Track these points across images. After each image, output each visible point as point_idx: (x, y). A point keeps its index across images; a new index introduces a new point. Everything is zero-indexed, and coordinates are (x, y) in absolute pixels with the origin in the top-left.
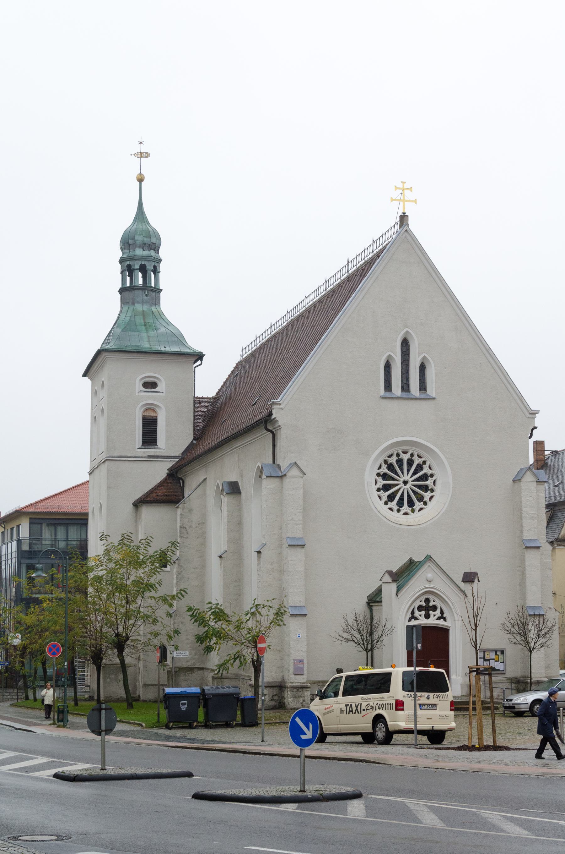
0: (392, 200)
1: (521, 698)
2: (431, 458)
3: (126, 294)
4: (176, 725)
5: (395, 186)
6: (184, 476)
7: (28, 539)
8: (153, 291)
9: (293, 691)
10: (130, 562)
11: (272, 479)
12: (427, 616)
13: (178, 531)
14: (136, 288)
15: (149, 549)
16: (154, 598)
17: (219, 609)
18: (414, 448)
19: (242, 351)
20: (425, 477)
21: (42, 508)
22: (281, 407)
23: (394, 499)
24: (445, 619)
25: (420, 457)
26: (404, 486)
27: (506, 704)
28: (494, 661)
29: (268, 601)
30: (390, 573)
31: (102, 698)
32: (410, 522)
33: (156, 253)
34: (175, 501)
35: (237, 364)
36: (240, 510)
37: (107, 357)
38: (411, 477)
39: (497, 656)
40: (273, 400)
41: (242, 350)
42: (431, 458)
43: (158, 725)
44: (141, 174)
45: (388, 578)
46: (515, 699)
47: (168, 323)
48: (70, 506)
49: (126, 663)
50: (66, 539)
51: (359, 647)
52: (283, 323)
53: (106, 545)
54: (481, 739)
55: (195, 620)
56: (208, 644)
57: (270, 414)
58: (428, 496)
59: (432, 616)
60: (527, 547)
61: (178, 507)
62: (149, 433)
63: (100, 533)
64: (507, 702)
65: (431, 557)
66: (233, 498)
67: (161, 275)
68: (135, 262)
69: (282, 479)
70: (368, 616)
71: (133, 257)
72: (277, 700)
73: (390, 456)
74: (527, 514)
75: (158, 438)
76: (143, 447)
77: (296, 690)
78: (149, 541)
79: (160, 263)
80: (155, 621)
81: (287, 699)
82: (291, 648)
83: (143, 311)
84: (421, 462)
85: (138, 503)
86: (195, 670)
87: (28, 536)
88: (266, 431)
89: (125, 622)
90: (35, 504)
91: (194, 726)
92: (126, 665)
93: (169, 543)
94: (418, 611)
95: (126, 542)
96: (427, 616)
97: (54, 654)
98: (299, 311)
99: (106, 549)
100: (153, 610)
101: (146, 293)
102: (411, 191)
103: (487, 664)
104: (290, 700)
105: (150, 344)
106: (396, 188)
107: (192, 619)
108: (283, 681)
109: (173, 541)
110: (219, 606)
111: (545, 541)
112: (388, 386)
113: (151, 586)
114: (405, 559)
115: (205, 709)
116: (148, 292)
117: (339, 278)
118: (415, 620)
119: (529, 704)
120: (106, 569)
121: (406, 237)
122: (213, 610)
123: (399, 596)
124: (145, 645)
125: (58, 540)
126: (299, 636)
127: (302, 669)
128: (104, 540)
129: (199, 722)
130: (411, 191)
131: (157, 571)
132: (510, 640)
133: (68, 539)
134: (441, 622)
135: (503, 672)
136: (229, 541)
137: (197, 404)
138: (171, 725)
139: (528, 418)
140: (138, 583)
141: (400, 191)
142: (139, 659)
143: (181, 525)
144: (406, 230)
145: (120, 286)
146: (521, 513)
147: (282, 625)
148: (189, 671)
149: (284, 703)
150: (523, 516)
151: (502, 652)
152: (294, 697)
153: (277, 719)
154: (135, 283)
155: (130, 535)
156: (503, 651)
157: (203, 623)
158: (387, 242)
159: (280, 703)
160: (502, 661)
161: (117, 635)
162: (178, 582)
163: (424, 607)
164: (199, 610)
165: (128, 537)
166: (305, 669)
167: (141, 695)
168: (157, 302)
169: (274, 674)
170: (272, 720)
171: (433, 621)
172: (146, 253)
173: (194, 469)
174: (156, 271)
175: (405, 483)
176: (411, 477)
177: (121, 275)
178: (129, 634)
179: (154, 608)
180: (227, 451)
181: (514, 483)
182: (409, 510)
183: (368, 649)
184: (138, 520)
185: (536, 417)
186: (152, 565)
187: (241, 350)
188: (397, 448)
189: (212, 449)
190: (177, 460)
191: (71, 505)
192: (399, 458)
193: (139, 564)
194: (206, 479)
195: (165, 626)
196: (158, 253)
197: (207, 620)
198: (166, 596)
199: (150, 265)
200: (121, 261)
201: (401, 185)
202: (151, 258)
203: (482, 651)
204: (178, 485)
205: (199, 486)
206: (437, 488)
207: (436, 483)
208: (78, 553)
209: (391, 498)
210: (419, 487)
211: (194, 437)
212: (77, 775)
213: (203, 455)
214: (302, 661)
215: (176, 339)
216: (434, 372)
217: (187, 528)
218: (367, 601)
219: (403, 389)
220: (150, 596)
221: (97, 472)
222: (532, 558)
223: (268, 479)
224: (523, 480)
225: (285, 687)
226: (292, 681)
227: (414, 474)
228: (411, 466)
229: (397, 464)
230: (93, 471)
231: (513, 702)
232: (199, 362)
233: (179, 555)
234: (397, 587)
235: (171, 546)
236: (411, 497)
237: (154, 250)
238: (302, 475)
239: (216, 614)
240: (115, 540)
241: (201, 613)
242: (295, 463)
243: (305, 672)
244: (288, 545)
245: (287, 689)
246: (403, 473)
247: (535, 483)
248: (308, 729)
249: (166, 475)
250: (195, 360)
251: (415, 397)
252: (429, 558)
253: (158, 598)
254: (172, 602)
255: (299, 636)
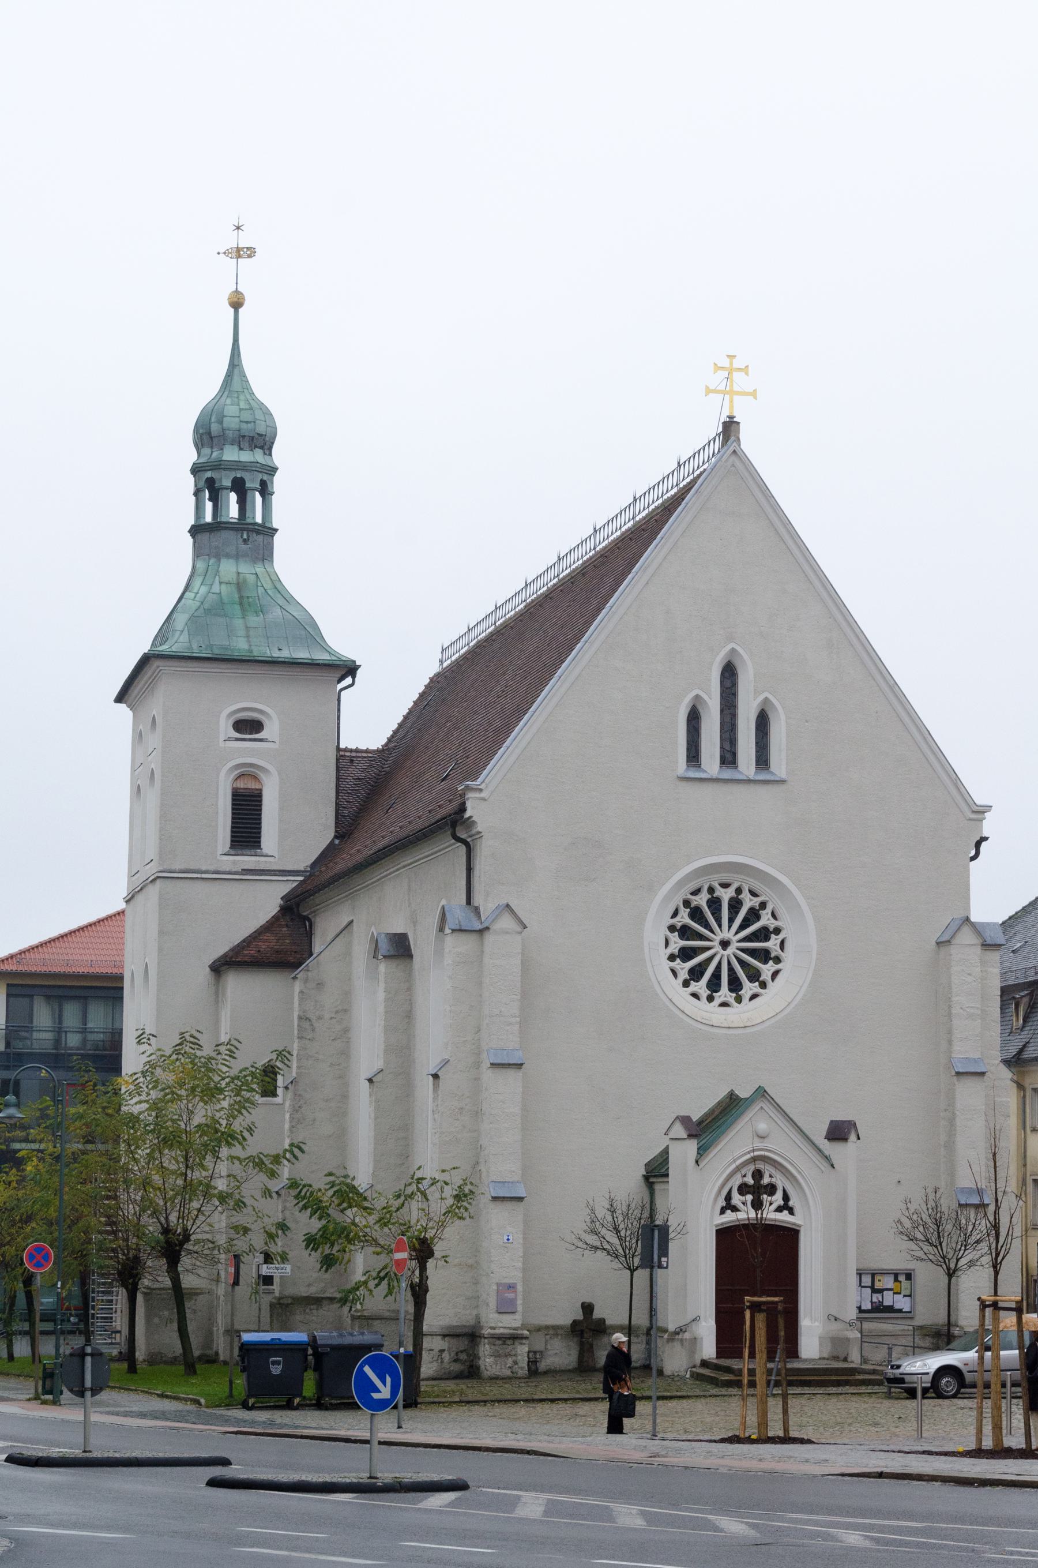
0: (708, 391)
1: (916, 1362)
2: (775, 897)
3: (204, 537)
4: (262, 1403)
5: (715, 364)
6: (312, 912)
7: (4, 1027)
8: (258, 532)
9: (494, 1345)
10: (193, 1089)
11: (463, 936)
12: (757, 1205)
13: (296, 1026)
14: (223, 525)
15: (232, 1062)
16: (238, 1159)
17: (347, 1185)
18: (743, 877)
19: (442, 653)
20: (764, 934)
21: (34, 965)
22: (482, 795)
23: (702, 976)
24: (791, 1211)
25: (754, 894)
26: (722, 952)
27: (889, 1374)
28: (891, 1293)
29: (443, 1171)
30: (685, 1120)
31: (140, 1355)
32: (732, 1022)
33: (265, 454)
34: (294, 962)
35: (432, 680)
36: (410, 989)
37: (163, 668)
38: (737, 933)
39: (897, 1284)
40: (468, 783)
41: (443, 650)
42: (775, 897)
43: (229, 1402)
44: (237, 292)
45: (679, 1131)
46: (906, 1364)
47: (289, 599)
48: (91, 961)
49: (183, 1286)
50: (83, 1028)
51: (616, 1264)
52: (550, 581)
53: (148, 1053)
54: (763, 1424)
55: (304, 1205)
56: (327, 1251)
57: (462, 809)
58: (769, 970)
59: (766, 1204)
60: (958, 1074)
61: (295, 978)
62: (243, 823)
63: (137, 1030)
64: (891, 1371)
65: (765, 1091)
66: (398, 965)
67: (276, 500)
68: (224, 473)
69: (482, 935)
70: (647, 1199)
71: (219, 463)
72: (466, 1361)
73: (696, 892)
74: (961, 1008)
75: (262, 833)
76: (233, 852)
77: (500, 1342)
78: (232, 1048)
79: (274, 475)
80: (240, 1205)
81: (483, 1359)
82: (492, 1261)
83: (238, 573)
84: (757, 904)
85: (221, 966)
86: (325, 1302)
87: (4, 1023)
88: (453, 841)
89: (183, 1204)
90: (18, 956)
91: (295, 1404)
92: (184, 1291)
93: (272, 1052)
94: (740, 1194)
95: (187, 1049)
96: (757, 1205)
97: (39, 1265)
98: (547, 584)
99: (149, 1062)
100: (238, 1184)
101: (245, 536)
102: (747, 374)
103: (877, 1298)
104: (489, 1360)
105: (249, 641)
106: (717, 368)
107: (298, 1203)
108: (478, 1325)
109: (280, 1049)
110: (349, 1181)
111: (997, 1062)
112: (694, 756)
113: (230, 1138)
114: (722, 1094)
115: (317, 1373)
116: (248, 534)
117: (660, 496)
118: (732, 1211)
119: (931, 1375)
120: (147, 1101)
121: (733, 465)
122: (335, 1189)
123: (701, 1166)
124: (219, 1250)
125: (66, 1032)
126: (508, 1240)
127: (513, 1302)
128: (144, 1043)
129: (304, 1398)
130: (747, 374)
131: (245, 1108)
132: (912, 1253)
133: (86, 1029)
134: (784, 1217)
135: (909, 1315)
136: (388, 1050)
137: (343, 763)
138: (251, 1401)
139: (970, 820)
140: (210, 1128)
141: (726, 374)
142: (218, 1281)
143: (302, 1014)
144: (734, 451)
145: (192, 521)
146: (950, 1007)
147: (468, 1218)
148: (313, 1304)
149: (478, 1368)
150: (954, 1011)
151: (909, 1277)
152: (497, 1355)
153: (455, 1395)
154: (221, 516)
155: (196, 1034)
156: (910, 1274)
157: (318, 1212)
158: (701, 469)
159: (471, 1366)
160: (908, 1294)
161: (166, 1231)
162: (293, 1127)
163: (750, 1186)
164: (310, 1186)
165: (192, 1040)
166: (519, 1302)
167: (221, 1352)
168: (265, 555)
169: (460, 1311)
170: (446, 1397)
171: (771, 1215)
172: (246, 456)
173: (331, 901)
174: (265, 491)
175: (725, 944)
176: (737, 933)
177: (194, 498)
178: (189, 1228)
179: (239, 1178)
180: (388, 872)
181: (939, 947)
182: (730, 997)
183: (633, 1266)
184: (220, 999)
185: (985, 819)
186: (238, 1095)
187: (441, 650)
188: (709, 877)
189: (362, 865)
190: (301, 878)
191: (94, 958)
192: (713, 897)
193: (211, 1093)
194: (352, 921)
195: (260, 1214)
196: (270, 455)
197: (326, 1206)
198: (261, 1156)
199: (253, 481)
200: (196, 470)
201: (725, 363)
202: (256, 464)
203: (868, 1273)
204: (301, 930)
205: (338, 935)
206: (787, 956)
207: (786, 945)
208: (91, 1068)
209: (696, 974)
210: (752, 952)
211: (336, 831)
212: (42, 1457)
213: (351, 872)
214: (513, 1287)
215: (303, 632)
216: (784, 729)
217: (314, 1021)
218: (645, 1173)
219: (723, 761)
220: (230, 1156)
221: (139, 898)
222: (969, 1094)
223: (455, 934)
224: (953, 942)
225: (480, 1337)
226: (493, 1325)
227: (742, 927)
228: (737, 913)
229: (709, 907)
230: (133, 897)
231: (901, 1370)
232: (348, 680)
233: (297, 1073)
234: (698, 1149)
235: (275, 1058)
236: (735, 973)
237: (262, 448)
238: (519, 929)
239: (342, 1195)
240: (168, 1043)
241: (315, 1194)
242: (508, 906)
243: (520, 1308)
244: (491, 1064)
245: (483, 1340)
246: (720, 926)
247: (978, 950)
248: (384, 1383)
249: (278, 909)
250: (340, 676)
251: (745, 778)
252: (761, 1093)
253: (245, 1159)
254: (275, 1168)
255: (508, 1240)
